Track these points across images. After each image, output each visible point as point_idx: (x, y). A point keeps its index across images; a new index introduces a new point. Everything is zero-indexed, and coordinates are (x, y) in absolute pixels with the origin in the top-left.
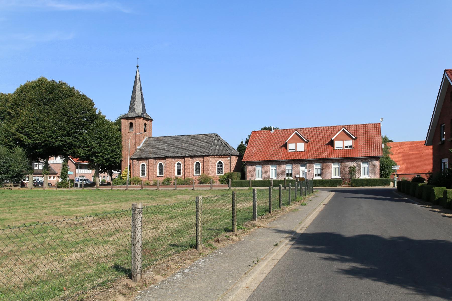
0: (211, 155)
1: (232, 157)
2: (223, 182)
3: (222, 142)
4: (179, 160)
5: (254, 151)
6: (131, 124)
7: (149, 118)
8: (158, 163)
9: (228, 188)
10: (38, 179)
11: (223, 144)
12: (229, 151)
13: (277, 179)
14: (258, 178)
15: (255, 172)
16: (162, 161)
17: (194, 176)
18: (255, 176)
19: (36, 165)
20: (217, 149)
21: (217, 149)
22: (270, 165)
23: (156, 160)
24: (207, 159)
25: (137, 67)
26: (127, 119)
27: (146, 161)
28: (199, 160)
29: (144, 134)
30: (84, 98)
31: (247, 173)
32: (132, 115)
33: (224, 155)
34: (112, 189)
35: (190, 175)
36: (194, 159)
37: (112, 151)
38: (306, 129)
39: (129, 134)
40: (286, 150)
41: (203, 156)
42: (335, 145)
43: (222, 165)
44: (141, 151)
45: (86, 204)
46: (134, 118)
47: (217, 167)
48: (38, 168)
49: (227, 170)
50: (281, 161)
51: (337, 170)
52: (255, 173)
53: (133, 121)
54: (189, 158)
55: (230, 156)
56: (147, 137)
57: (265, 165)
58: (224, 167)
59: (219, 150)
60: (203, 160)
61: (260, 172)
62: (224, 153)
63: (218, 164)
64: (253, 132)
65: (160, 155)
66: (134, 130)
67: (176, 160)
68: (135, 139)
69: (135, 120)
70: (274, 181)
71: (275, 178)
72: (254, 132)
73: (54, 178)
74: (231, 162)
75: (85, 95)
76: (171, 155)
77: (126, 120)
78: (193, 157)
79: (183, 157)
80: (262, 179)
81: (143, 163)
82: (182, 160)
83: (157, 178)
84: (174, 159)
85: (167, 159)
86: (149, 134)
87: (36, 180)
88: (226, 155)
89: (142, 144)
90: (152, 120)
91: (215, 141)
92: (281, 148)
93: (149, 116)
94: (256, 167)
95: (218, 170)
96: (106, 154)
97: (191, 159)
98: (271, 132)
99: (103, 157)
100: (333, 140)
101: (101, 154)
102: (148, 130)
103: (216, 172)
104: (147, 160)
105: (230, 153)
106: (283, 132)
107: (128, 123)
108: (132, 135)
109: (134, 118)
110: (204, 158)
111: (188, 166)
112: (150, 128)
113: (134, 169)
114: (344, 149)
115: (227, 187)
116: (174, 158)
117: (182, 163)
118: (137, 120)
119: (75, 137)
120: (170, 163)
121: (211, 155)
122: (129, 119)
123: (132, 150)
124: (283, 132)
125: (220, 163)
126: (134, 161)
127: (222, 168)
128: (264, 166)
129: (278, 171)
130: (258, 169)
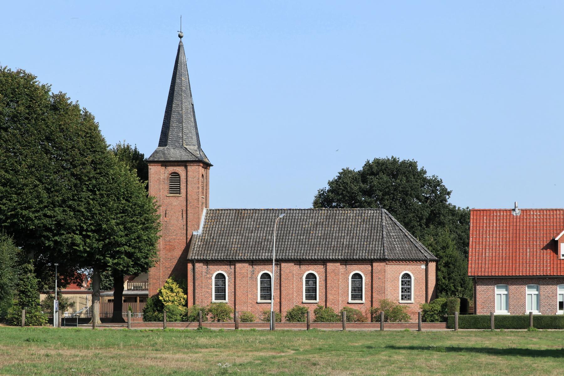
0: (389, 260)
2: (434, 318)
5: (487, 254)
13: (540, 314)
14: (501, 311)
16: (316, 270)
17: (257, 303)
18: (494, 306)
20: (398, 249)
21: (398, 249)
24: (379, 268)
25: (180, 37)
26: (165, 163)
28: (361, 270)
30: (88, 117)
32: (174, 154)
33: (395, 260)
34: (273, 329)
35: (340, 302)
36: (348, 266)
38: (298, 211)
39: (168, 200)
40: (555, 255)
41: (371, 262)
42: (560, 250)
43: (410, 282)
44: (207, 244)
46: (184, 163)
47: (400, 287)
49: (419, 292)
50: (549, 278)
51: (534, 298)
52: (494, 301)
53: (180, 170)
54: (339, 264)
57: (515, 284)
60: (370, 268)
62: (413, 256)
63: (402, 278)
66: (183, 191)
67: (303, 267)
69: (186, 167)
71: (536, 312)
76: (292, 255)
78: (345, 262)
79: (324, 262)
80: (509, 314)
81: (311, 272)
82: (321, 268)
83: (257, 306)
84: (300, 265)
88: (419, 261)
92: (545, 251)
94: (558, 288)
97: (341, 267)
98: (515, 215)
99: (130, 255)
100: (557, 241)
104: (230, 265)
106: (540, 215)
107: (166, 175)
108: (177, 202)
109: (184, 163)
110: (235, 265)
111: (336, 281)
113: (197, 284)
114: (560, 260)
115: (443, 328)
116: (300, 262)
117: (319, 274)
120: (291, 275)
121: (389, 260)
122: (169, 164)
123: (178, 238)
124: (540, 215)
125: (407, 276)
127: (409, 289)
129: (542, 297)
130: (500, 292)
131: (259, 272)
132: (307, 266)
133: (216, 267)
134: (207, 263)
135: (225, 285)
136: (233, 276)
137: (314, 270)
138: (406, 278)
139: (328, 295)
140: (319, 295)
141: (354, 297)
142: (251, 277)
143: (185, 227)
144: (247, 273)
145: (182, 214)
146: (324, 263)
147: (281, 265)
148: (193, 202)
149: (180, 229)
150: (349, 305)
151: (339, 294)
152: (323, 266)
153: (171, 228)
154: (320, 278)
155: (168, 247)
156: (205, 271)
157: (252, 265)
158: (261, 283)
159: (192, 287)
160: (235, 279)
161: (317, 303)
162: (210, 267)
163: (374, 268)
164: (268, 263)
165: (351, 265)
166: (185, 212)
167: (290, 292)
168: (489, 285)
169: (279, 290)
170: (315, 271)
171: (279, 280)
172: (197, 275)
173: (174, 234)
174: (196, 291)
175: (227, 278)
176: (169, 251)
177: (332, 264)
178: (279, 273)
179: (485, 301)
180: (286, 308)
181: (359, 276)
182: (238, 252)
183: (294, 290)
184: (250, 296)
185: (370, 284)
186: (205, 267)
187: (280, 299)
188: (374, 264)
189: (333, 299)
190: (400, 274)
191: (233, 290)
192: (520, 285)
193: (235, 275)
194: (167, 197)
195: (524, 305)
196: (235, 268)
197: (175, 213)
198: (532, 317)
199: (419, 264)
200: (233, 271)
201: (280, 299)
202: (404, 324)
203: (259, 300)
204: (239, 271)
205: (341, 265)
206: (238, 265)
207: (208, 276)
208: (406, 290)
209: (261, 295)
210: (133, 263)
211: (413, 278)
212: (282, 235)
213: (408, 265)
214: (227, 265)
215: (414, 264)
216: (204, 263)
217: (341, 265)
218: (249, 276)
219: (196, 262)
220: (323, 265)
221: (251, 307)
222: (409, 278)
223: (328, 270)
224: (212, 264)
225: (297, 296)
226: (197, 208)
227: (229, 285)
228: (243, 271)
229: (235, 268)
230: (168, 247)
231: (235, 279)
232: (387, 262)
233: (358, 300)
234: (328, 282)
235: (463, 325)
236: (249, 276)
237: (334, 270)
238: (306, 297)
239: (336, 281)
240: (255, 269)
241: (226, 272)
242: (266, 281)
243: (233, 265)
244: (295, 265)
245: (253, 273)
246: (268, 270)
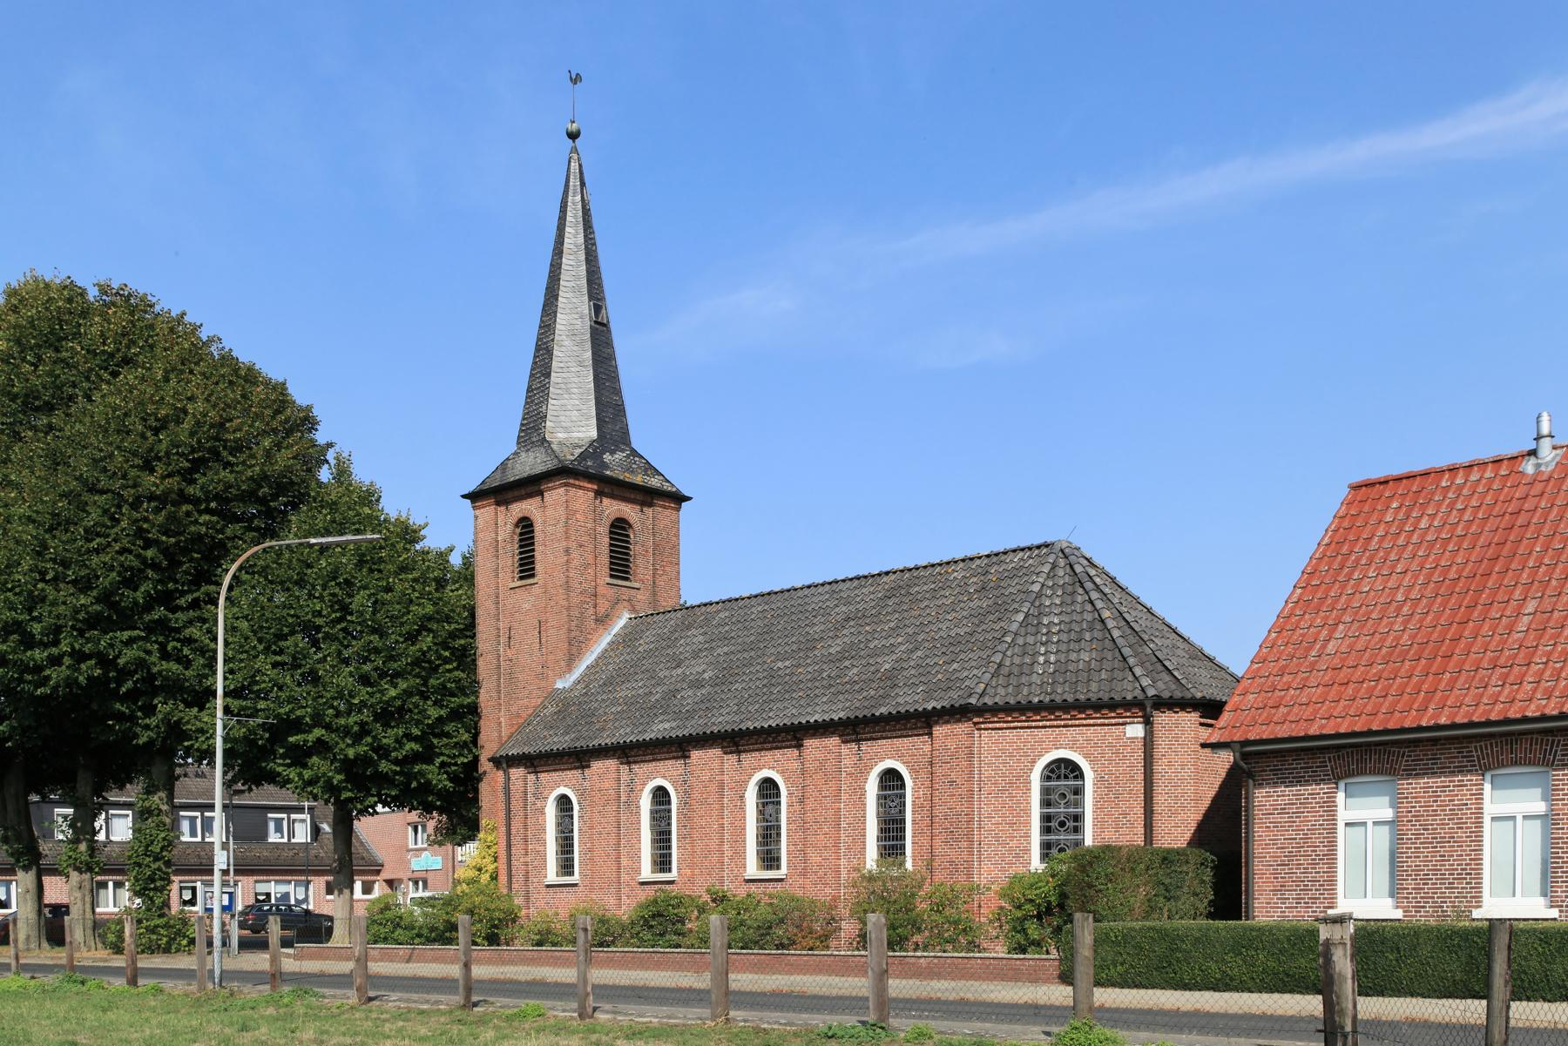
0: (982, 711)
1: (1162, 719)
3: (1099, 604)
6: (620, 528)
7: (655, 482)
8: (644, 784)
9: (1060, 994)
10: (286, 896)
11: (1106, 614)
12: (1138, 671)
13: (1554, 913)
15: (1332, 844)
19: (279, 822)
21: (1045, 660)
22: (1483, 769)
23: (635, 767)
25: (573, 136)
27: (577, 773)
28: (899, 756)
29: (611, 592)
31: (1257, 850)
36: (865, 746)
37: (386, 716)
41: (921, 722)
43: (1078, 791)
44: (565, 706)
48: (285, 840)
53: (629, 511)
54: (833, 741)
55: (1145, 708)
56: (633, 610)
58: (1096, 809)
59: (1061, 669)
60: (927, 748)
61: (1379, 841)
62: (1095, 691)
64: (1356, 487)
65: (661, 728)
67: (748, 759)
70: (1516, 932)
72: (1369, 484)
73: (367, 889)
74: (1159, 767)
75: (257, 367)
76: (721, 721)
77: (498, 504)
78: (855, 729)
80: (1399, 914)
84: (739, 752)
86: (654, 594)
87: (273, 901)
88: (1112, 705)
89: (589, 659)
90: (678, 499)
91: (1039, 595)
93: (650, 469)
95: (1046, 830)
96: (346, 731)
97: (846, 749)
101: (318, 732)
102: (642, 565)
103: (1027, 851)
105: (1145, 682)
107: (510, 527)
108: (527, 601)
109: (531, 486)
112: (668, 551)
117: (786, 780)
118: (556, 495)
119: (162, 626)
120: (713, 787)
121: (982, 711)
122: (510, 495)
125: (1065, 770)
128: (1417, 787)
133: (555, 775)
134: (533, 765)
137: (773, 768)
138: (1066, 777)
151: (836, 845)
161: (781, 880)
168: (1307, 783)
170: (778, 771)
179: (1290, 855)
183: (726, 836)
186: (531, 777)
189: (820, 866)
190: (1034, 762)
192: (1453, 773)
195: (1471, 874)
199: (1113, 721)
202: (913, 960)
205: (843, 742)
208: (1062, 824)
211: (1089, 775)
213: (1064, 726)
214: (576, 768)
215: (1092, 722)
232: (975, 720)
235: (1119, 968)
244: (726, 753)
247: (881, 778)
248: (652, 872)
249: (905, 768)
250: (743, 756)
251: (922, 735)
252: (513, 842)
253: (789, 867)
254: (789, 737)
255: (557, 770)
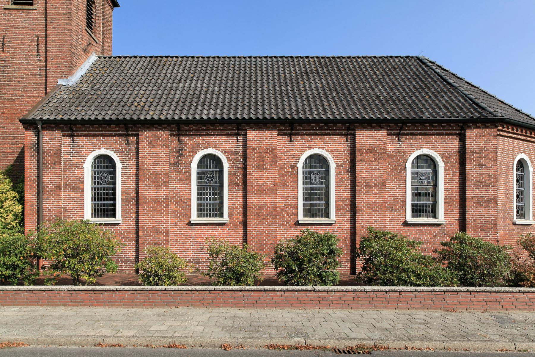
4: (318, 140)
17: (190, 224)
23: (185, 139)
24: (481, 142)
28: (434, 148)
36: (403, 139)
45: (196, 128)
54: (382, 133)
67: (298, 141)
68: (42, 42)
81: (103, 151)
83: (189, 230)
85: (251, 134)
102: (98, 29)
104: (127, 136)
110: (137, 135)
111: (377, 173)
113: (46, 179)
117: (335, 157)
123: (29, 93)
126: (48, 135)
131: (194, 152)
132: (308, 137)
133: (94, 140)
134: (71, 129)
135: (115, 183)
136: (134, 161)
137: (323, 148)
139: (360, 206)
140: (337, 206)
141: (417, 210)
142: (176, 165)
143: (43, 72)
144: (167, 154)
145: (38, 45)
146: (348, 129)
147: (246, 135)
148: (58, 20)
149: (34, 75)
150: (406, 228)
152: (344, 139)
153: (15, 74)
154: (338, 167)
155: (8, 113)
156: (68, 149)
157: (178, 135)
158: (200, 178)
159: (35, 185)
160: (137, 169)
162: (80, 140)
163: (468, 141)
164: (215, 130)
165: (412, 134)
166: (44, 42)
167: (270, 198)
169: (241, 194)
170: (327, 150)
171: (240, 170)
172: (46, 158)
173: (22, 85)
174: (45, 196)
175: (119, 166)
176: (11, 121)
177: (367, 133)
178: (241, 153)
180: (258, 236)
181: (430, 161)
182: (147, 108)
184: (172, 207)
185: (456, 179)
186: (68, 139)
187: (245, 215)
188: (471, 134)
189: (371, 216)
191: (134, 194)
193: (138, 158)
194: (7, 11)
196: (137, 143)
197: (23, 43)
198: (306, 219)
200: (133, 149)
201: (245, 215)
203: (194, 218)
204: (147, 150)
206: (145, 135)
207: (75, 161)
209: (199, 205)
210: (459, 282)
212: (248, 69)
214: (120, 135)
216: (63, 131)
217: (388, 135)
218: (171, 161)
219: (43, 128)
220: (346, 135)
221: (176, 234)
222: (521, 170)
223: (358, 147)
224: (84, 133)
225: (283, 208)
226: (68, 33)
227: (123, 183)
228: (157, 150)
229: (137, 143)
230: (8, 113)
231: (137, 169)
233: (427, 217)
234: (360, 174)
236: (171, 161)
237: (373, 146)
238: (305, 210)
239: (377, 173)
240: (186, 145)
241: (116, 151)
242: (210, 172)
243: (132, 135)
245: (180, 154)
246: (215, 148)
247: (95, 160)
248: (198, 217)
249: (438, 155)
250: (294, 138)
251: (451, 135)
252: (35, 198)
253: (337, 215)
254: (343, 128)
255: (98, 136)
